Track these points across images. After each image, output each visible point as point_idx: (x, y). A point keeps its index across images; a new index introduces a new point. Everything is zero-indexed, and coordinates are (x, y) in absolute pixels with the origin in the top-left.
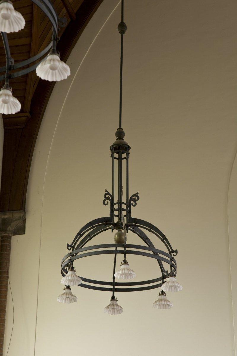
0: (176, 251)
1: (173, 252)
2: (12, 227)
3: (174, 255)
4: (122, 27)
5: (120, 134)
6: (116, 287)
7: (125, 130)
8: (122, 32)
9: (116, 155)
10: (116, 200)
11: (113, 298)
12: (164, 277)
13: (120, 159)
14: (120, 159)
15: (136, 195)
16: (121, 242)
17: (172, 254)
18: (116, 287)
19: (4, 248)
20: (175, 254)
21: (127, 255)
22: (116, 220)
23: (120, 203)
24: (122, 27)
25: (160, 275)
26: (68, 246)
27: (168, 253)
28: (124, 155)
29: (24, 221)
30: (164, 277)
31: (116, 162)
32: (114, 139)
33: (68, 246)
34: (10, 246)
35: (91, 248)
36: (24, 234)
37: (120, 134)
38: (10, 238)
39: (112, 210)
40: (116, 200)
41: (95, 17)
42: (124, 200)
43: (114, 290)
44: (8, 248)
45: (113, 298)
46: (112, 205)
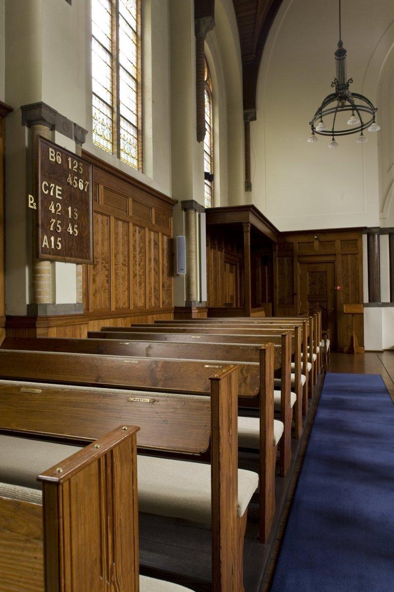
0: (377, 109)
1: (375, 109)
5: (340, 44)
6: (335, 134)
7: (343, 41)
11: (333, 139)
12: (362, 126)
15: (351, 79)
16: (343, 106)
18: (335, 134)
19: (39, 275)
25: (360, 125)
29: (256, 113)
30: (362, 126)
32: (336, 48)
34: (249, 126)
36: (256, 120)
37: (340, 44)
38: (249, 122)
41: (269, 37)
43: (333, 135)
45: (333, 139)
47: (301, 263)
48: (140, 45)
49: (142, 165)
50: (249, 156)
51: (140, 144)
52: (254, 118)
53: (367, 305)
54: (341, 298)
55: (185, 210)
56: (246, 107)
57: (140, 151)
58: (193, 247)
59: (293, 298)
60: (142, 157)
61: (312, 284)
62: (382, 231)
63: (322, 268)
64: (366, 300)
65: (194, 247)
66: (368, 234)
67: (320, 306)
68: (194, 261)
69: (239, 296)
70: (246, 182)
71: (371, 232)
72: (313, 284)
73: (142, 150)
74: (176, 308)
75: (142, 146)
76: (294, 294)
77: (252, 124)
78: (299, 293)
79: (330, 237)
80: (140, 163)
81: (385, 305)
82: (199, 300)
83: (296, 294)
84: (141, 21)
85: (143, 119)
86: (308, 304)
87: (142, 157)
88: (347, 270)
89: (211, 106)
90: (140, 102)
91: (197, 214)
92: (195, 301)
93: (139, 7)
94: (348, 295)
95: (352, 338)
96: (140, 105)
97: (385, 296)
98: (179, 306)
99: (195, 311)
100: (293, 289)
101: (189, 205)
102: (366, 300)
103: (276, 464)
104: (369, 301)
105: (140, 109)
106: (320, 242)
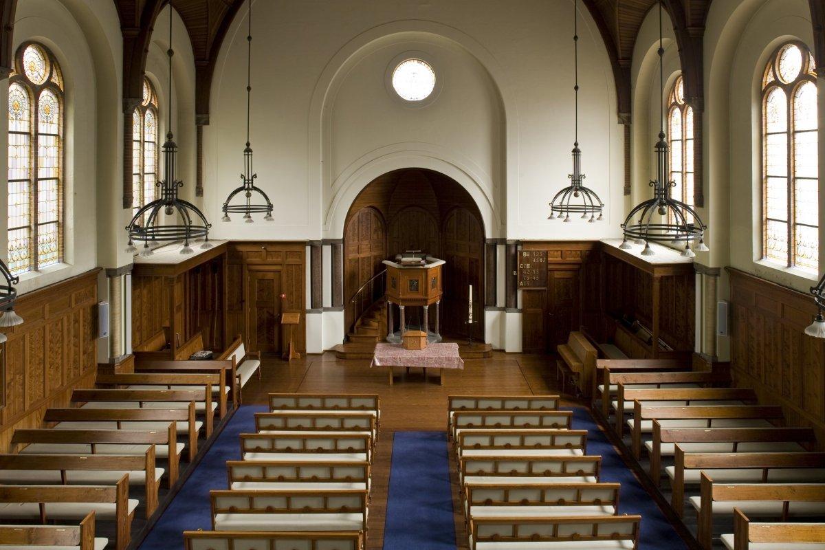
2: (203, 121)
3: (14, 283)
4: (249, 38)
8: (249, 91)
9: (246, 153)
10: (247, 179)
13: (248, 155)
14: (248, 155)
17: (12, 282)
20: (16, 281)
21: (40, 176)
22: (246, 187)
23: (248, 180)
24: (249, 38)
26: (621, 225)
27: (153, 208)
28: (250, 153)
29: (209, 118)
31: (247, 156)
33: (621, 225)
35: (492, 277)
38: (201, 127)
39: (245, 183)
40: (247, 179)
41: (233, 24)
42: (250, 178)
44: (619, 10)
46: (245, 180)
47: (250, 271)
48: (61, 145)
49: (63, 254)
50: (201, 168)
51: (61, 236)
52: (207, 123)
53: (309, 312)
54: (286, 305)
55: (110, 276)
56: (198, 112)
57: (61, 242)
58: (117, 310)
59: (242, 305)
60: (63, 247)
61: (261, 291)
62: (325, 242)
63: (270, 276)
64: (308, 306)
65: (120, 308)
66: (311, 246)
67: (267, 312)
68: (117, 322)
69: (188, 303)
70: (197, 188)
71: (315, 246)
72: (261, 290)
73: (63, 240)
74: (99, 365)
75: (63, 237)
76: (242, 301)
77: (205, 128)
78: (247, 298)
79: (278, 248)
80: (61, 253)
81: (327, 309)
82: (123, 353)
83: (244, 301)
84: (64, 124)
85: (64, 212)
86: (256, 310)
87: (63, 247)
88: (292, 279)
89: (156, 122)
90: (61, 197)
91: (123, 276)
92: (118, 358)
93: (62, 111)
94: (292, 303)
95: (289, 344)
96: (61, 201)
97: (327, 302)
98: (103, 362)
99: (117, 367)
100: (242, 296)
101: (112, 273)
102: (308, 306)
103: (132, 525)
104: (312, 307)
105: (61, 204)
106: (267, 251)
